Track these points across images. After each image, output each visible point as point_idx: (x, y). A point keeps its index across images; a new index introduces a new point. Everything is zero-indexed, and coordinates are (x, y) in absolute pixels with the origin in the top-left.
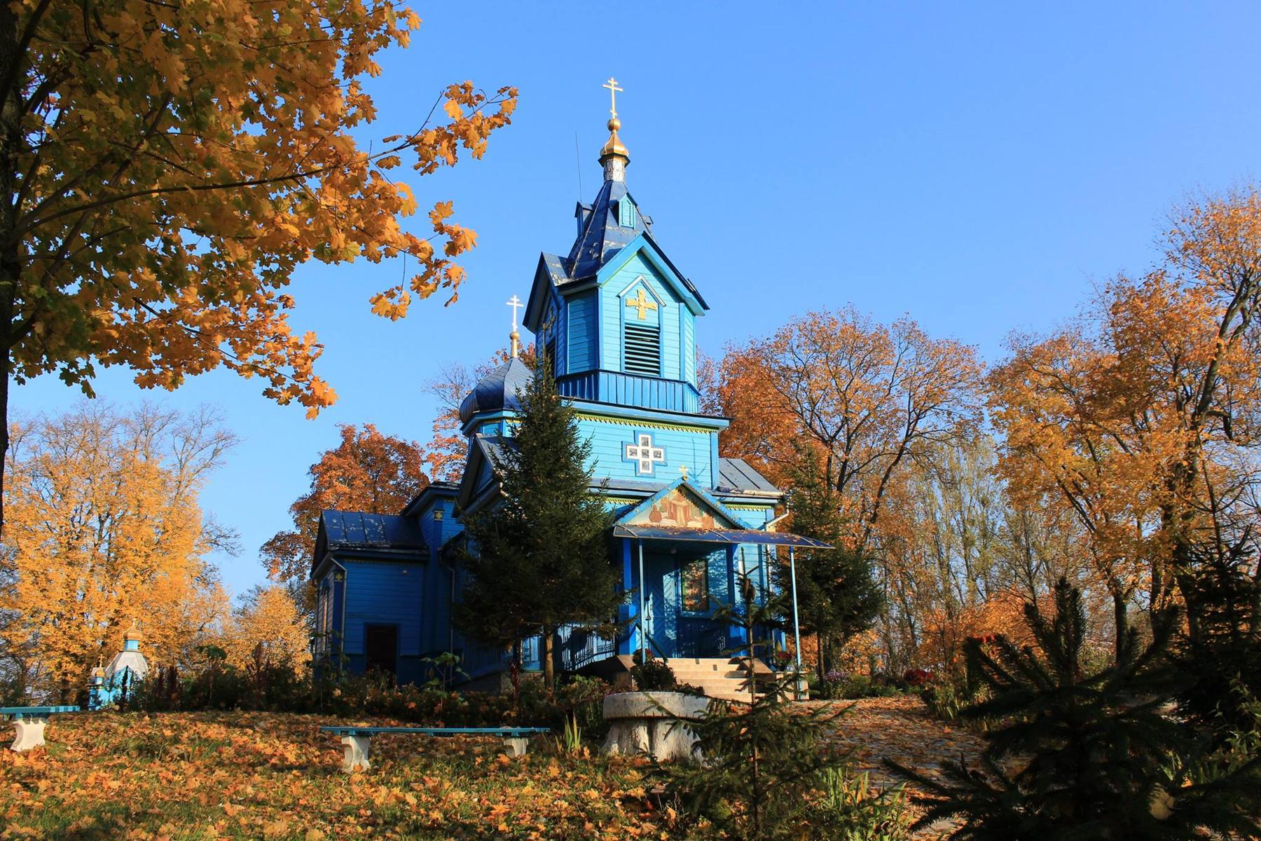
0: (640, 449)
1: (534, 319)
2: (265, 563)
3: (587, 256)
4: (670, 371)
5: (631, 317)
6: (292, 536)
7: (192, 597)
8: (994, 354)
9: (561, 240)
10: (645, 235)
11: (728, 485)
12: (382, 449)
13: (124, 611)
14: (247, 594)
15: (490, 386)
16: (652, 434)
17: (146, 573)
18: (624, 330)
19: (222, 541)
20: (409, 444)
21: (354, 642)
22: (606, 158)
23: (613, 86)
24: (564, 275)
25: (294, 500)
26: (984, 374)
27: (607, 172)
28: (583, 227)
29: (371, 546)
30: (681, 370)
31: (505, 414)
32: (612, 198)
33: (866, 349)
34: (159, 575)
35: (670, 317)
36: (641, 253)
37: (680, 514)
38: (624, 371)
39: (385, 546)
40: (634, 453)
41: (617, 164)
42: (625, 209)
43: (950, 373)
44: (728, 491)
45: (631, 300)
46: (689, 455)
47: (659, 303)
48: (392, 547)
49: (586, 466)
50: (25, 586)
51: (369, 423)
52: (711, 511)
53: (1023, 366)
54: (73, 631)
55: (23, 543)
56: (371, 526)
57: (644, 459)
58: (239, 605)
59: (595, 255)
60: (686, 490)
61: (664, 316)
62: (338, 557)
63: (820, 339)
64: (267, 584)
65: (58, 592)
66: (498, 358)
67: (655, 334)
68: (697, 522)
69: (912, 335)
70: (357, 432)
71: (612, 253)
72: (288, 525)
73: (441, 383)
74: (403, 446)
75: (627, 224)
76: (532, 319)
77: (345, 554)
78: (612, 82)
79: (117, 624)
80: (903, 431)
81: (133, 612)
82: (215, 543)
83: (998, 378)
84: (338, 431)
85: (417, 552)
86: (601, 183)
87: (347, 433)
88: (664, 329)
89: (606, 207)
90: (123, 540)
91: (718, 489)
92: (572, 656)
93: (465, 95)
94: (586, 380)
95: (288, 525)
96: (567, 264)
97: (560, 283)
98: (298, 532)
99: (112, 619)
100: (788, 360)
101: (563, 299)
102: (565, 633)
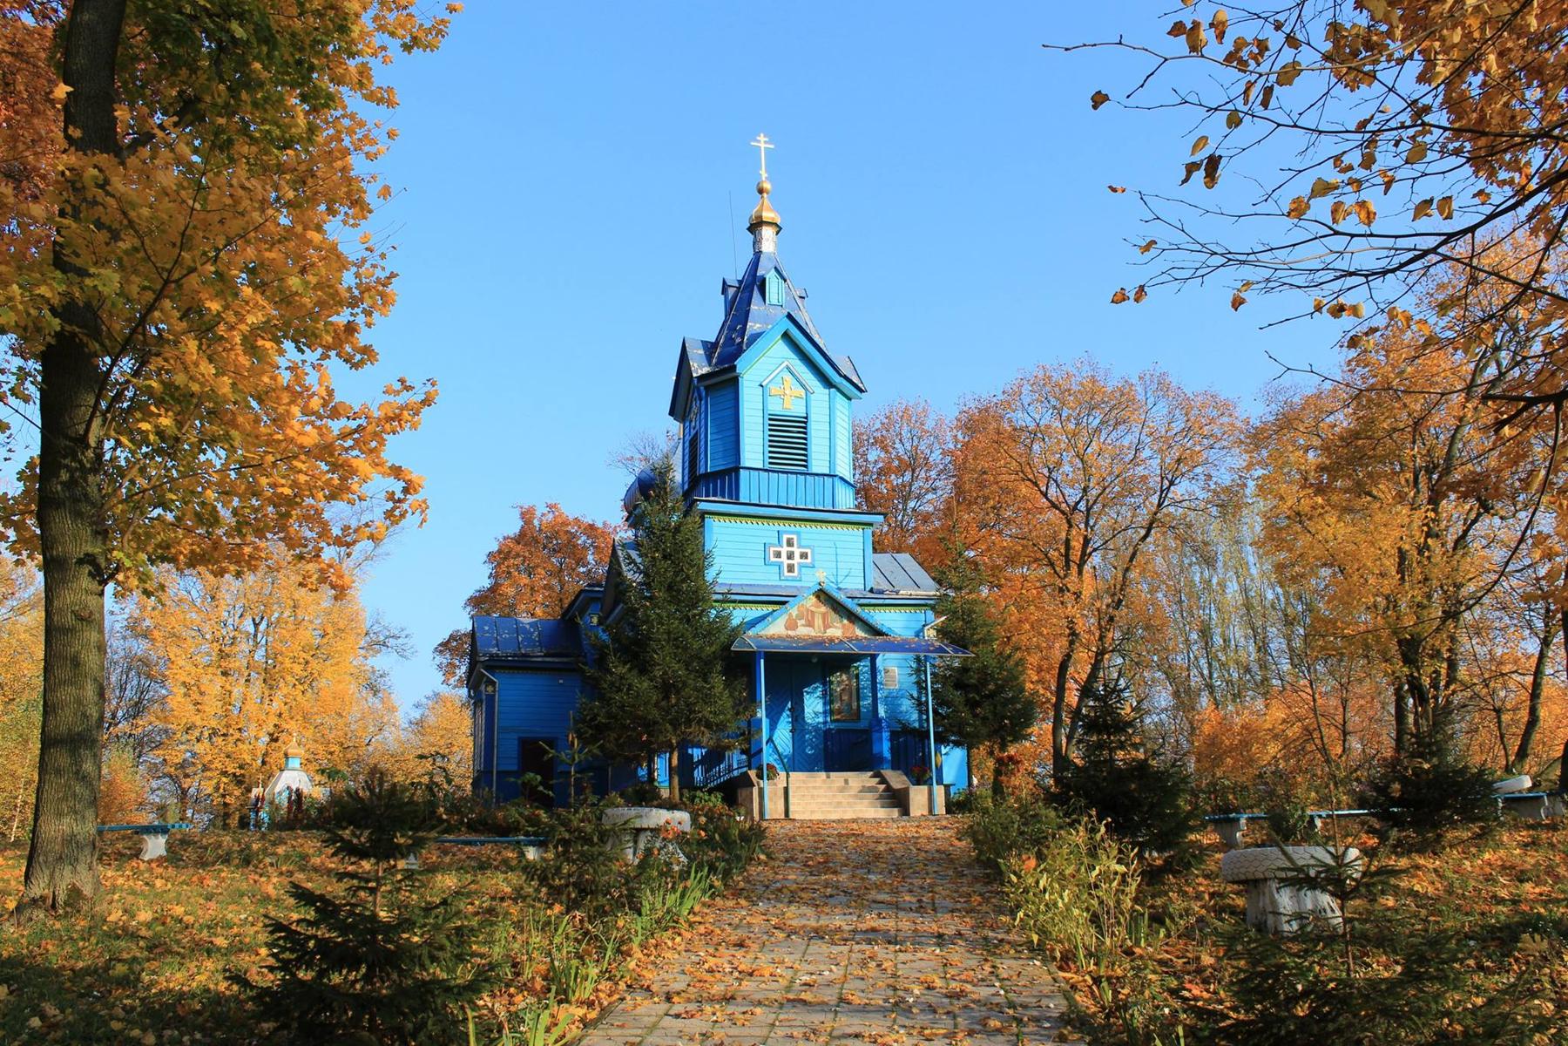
0: (784, 550)
1: (679, 409)
3: (730, 340)
4: (818, 464)
5: (775, 407)
7: (360, 704)
8: (1255, 411)
9: (709, 323)
10: (789, 316)
11: (884, 586)
12: (568, 532)
13: (284, 726)
14: (424, 701)
16: (798, 534)
17: (307, 681)
19: (391, 642)
20: (599, 525)
21: (507, 755)
22: (755, 226)
23: (762, 142)
24: (705, 363)
25: (470, 592)
27: (757, 242)
28: (730, 306)
30: (832, 463)
33: (1116, 407)
34: (323, 683)
36: (786, 336)
37: (818, 621)
38: (768, 466)
39: (538, 654)
40: (778, 555)
41: (767, 233)
42: (773, 285)
43: (1206, 430)
44: (882, 592)
46: (842, 557)
49: (710, 575)
50: (177, 700)
52: (853, 617)
53: (1286, 422)
54: (230, 748)
55: (173, 651)
57: (778, 568)
58: (416, 714)
60: (823, 595)
61: (813, 404)
62: (490, 668)
63: (1054, 392)
64: (445, 690)
65: (212, 706)
68: (838, 630)
69: (1163, 386)
70: (538, 514)
71: (755, 337)
74: (592, 527)
76: (679, 408)
77: (495, 664)
78: (762, 138)
79: (276, 740)
81: (292, 726)
82: (384, 644)
83: (1257, 438)
84: (517, 513)
86: (750, 256)
87: (527, 515)
88: (812, 417)
89: (753, 284)
90: (279, 646)
91: (871, 591)
93: (402, 381)
94: (725, 479)
96: (710, 348)
97: (700, 372)
99: (271, 735)
100: (1021, 419)
101: (706, 390)
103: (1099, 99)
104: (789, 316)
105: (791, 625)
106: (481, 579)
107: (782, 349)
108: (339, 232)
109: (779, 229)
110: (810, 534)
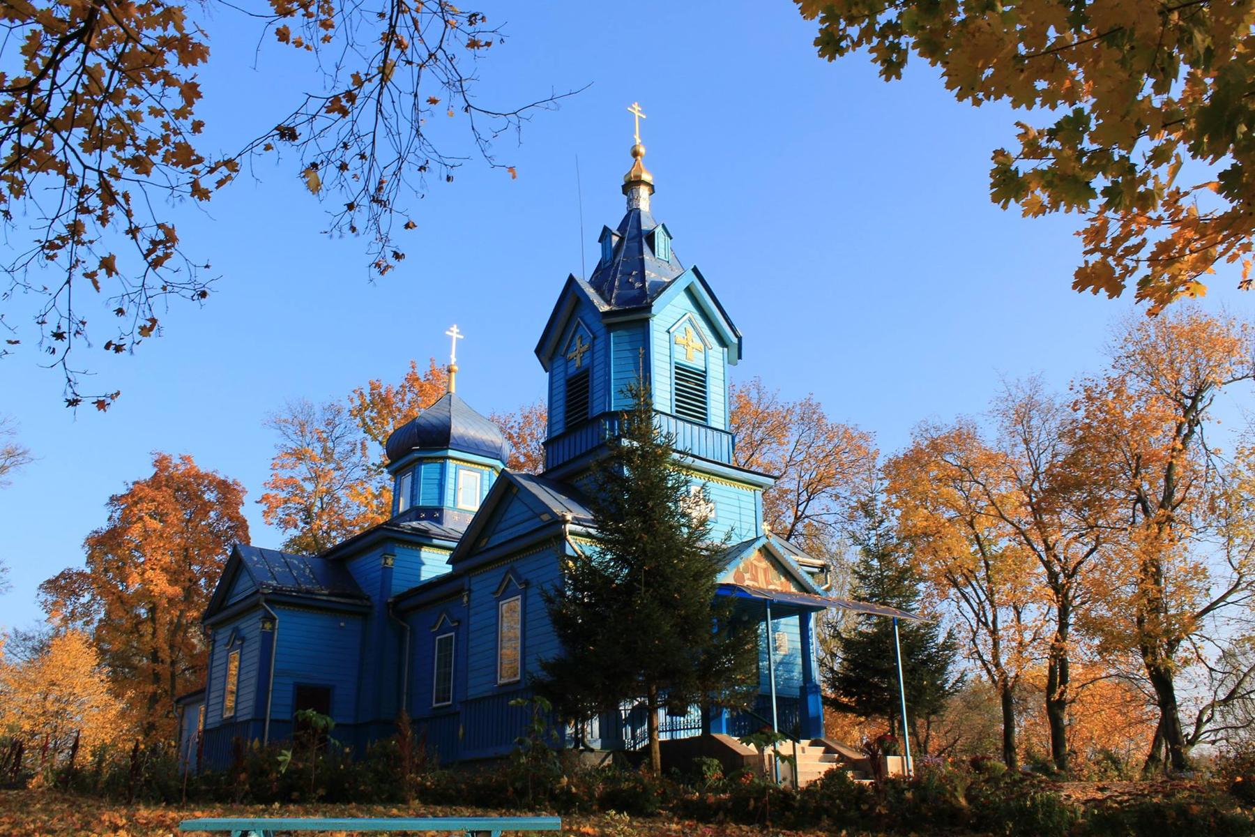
2: (45, 603)
5: (680, 358)
6: (81, 574)
8: (893, 442)
10: (695, 270)
15: (434, 421)
18: (674, 370)
20: (230, 481)
22: (631, 185)
26: (881, 462)
29: (308, 591)
31: (451, 453)
32: (644, 227)
35: (714, 361)
36: (689, 291)
41: (644, 191)
45: (679, 336)
47: (705, 345)
48: (329, 595)
51: (187, 454)
56: (298, 568)
59: (638, 285)
61: (711, 359)
62: (267, 601)
66: (355, 396)
67: (700, 378)
69: (811, 416)
72: (78, 561)
73: (284, 417)
75: (662, 257)
78: (636, 106)
80: (791, 513)
85: (358, 602)
88: (710, 374)
92: (633, 732)
95: (78, 561)
98: (88, 571)
102: (625, 708)
103: (207, 266)
104: (695, 270)
106: (101, 521)
107: (684, 302)
109: (652, 188)
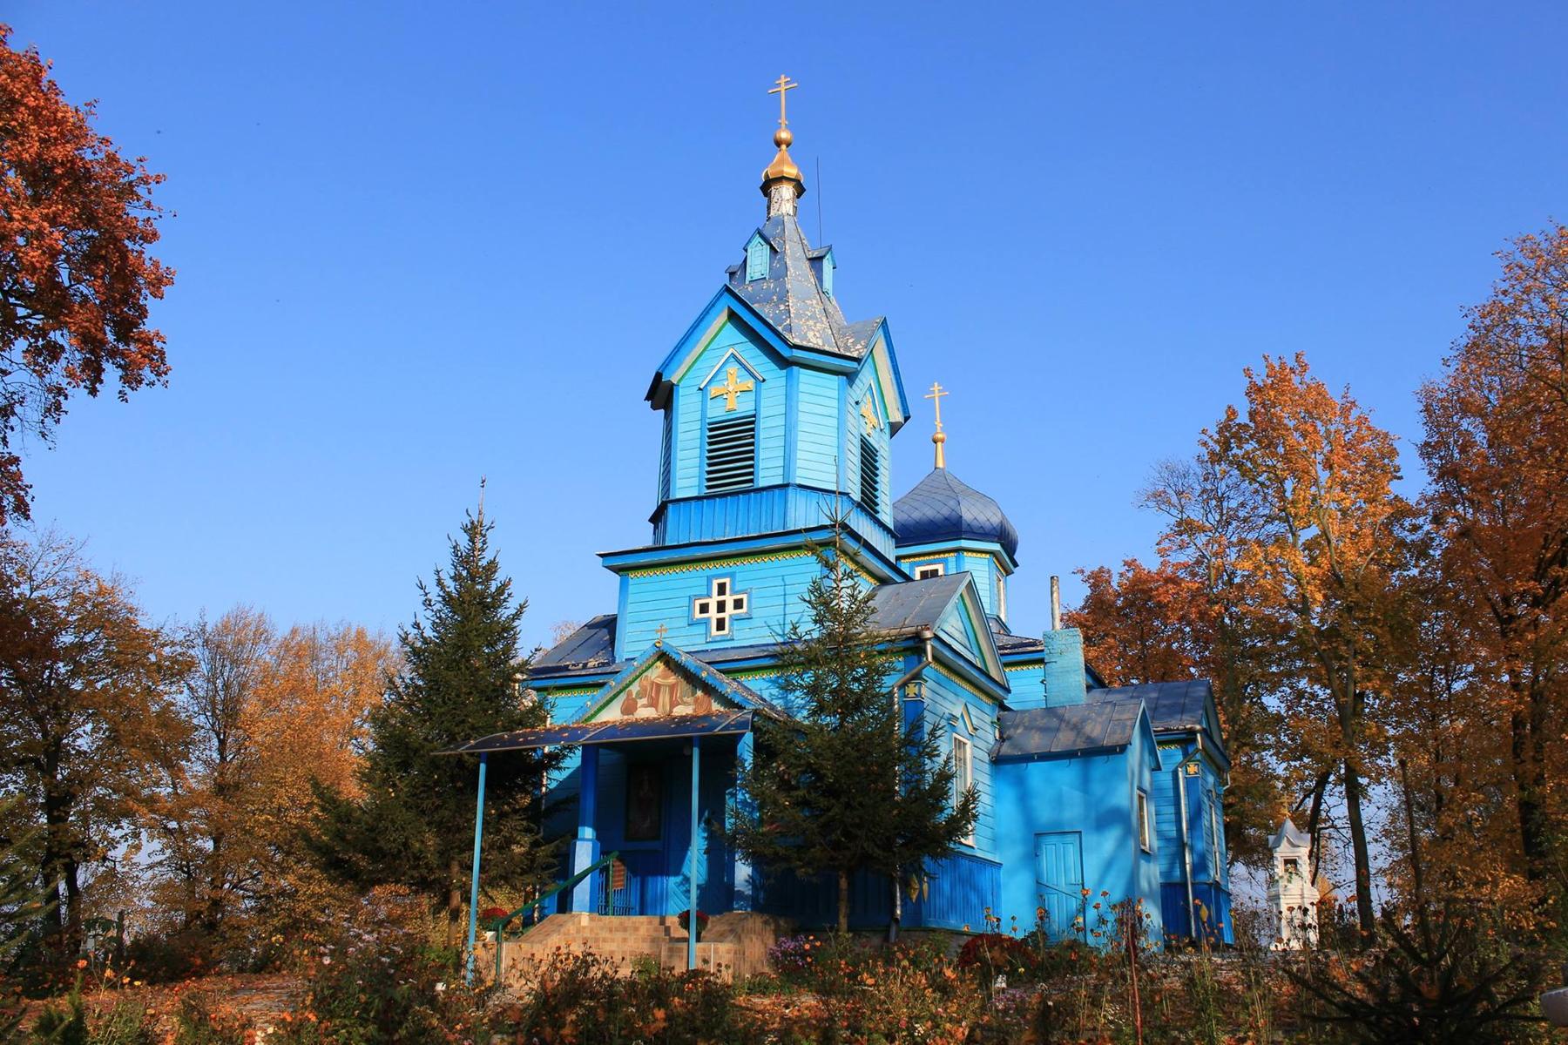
16: (732, 575)
37: (664, 698)
52: (709, 690)
88: (763, 412)
105: (629, 708)
107: (732, 334)
108: (265, 655)
110: (747, 573)
